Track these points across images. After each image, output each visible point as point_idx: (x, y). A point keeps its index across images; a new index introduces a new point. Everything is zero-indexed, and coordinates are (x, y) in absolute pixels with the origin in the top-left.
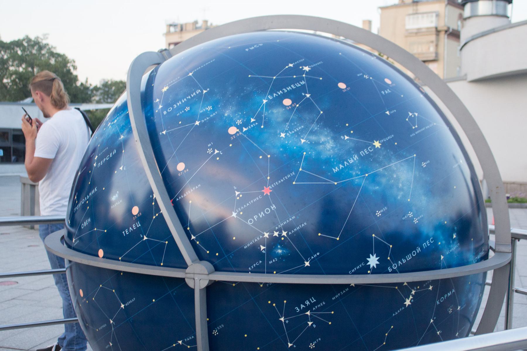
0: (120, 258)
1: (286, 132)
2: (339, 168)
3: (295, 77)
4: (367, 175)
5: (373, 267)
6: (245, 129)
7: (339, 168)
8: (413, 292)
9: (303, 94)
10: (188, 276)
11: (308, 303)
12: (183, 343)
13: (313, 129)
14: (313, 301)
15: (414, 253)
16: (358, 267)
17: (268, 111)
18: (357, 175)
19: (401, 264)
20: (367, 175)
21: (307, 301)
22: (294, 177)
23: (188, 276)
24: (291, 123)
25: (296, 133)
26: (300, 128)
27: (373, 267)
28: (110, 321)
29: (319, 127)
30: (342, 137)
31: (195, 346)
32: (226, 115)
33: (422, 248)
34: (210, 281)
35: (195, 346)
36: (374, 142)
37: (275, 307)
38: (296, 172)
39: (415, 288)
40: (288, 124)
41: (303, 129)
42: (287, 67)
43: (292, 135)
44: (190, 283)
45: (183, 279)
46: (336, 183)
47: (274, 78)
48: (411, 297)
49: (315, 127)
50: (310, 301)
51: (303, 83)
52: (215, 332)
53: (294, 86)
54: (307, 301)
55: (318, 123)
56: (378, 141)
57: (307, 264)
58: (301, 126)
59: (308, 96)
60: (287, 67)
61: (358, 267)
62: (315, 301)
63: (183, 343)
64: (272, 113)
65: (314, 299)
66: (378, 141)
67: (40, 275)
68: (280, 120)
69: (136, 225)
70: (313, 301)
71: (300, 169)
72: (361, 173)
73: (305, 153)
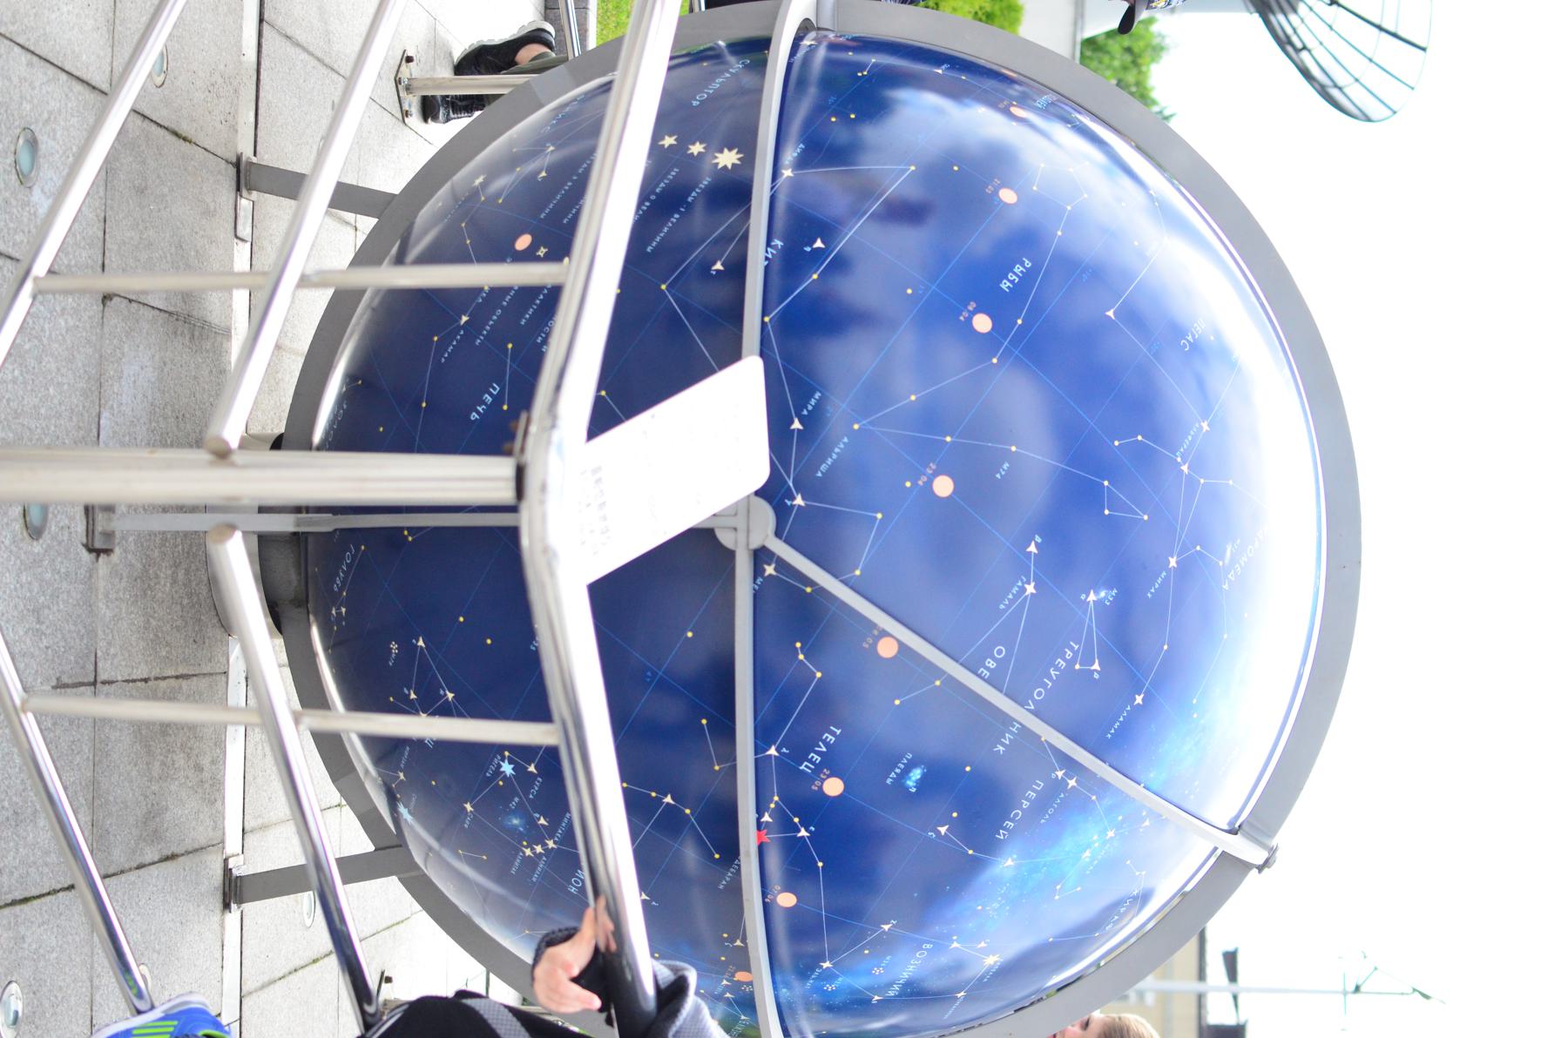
0: (603, 393)
5: (737, 153)
11: (1001, 748)
12: (796, 508)
14: (806, 766)
19: (817, 749)
21: (989, 660)
27: (737, 153)
28: (466, 322)
31: (716, 367)
35: (716, 367)
37: (816, 680)
50: (1034, 790)
52: (767, 319)
53: (814, 760)
54: (989, 660)
62: (802, 767)
63: (796, 508)
65: (806, 769)
67: (369, 51)
69: (813, 763)
70: (806, 766)
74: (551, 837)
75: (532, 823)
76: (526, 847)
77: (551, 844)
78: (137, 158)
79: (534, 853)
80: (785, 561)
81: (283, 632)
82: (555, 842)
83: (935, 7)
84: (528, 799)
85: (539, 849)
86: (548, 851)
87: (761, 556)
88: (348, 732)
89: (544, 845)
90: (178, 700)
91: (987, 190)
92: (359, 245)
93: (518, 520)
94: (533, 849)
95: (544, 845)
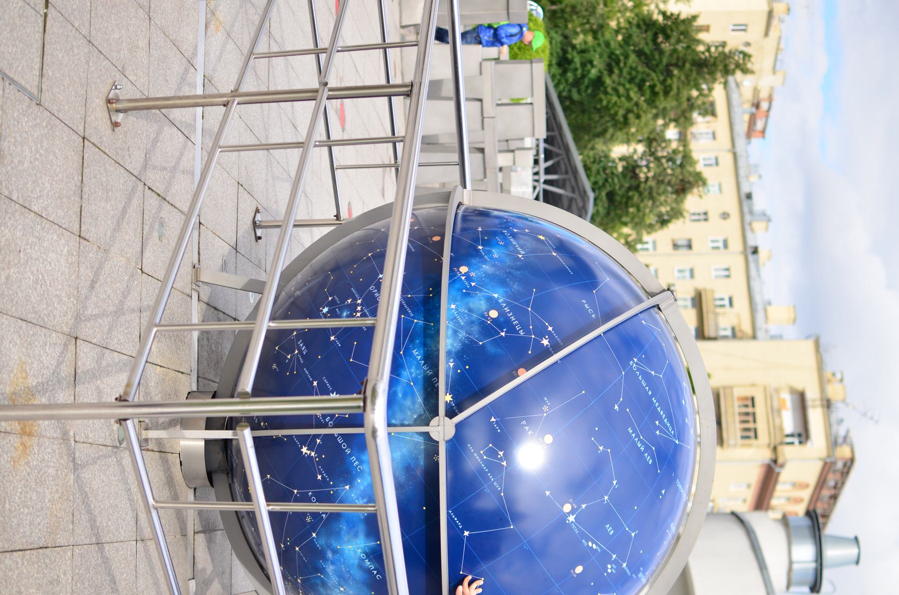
1: (456, 310)
2: (417, 355)
3: (531, 327)
4: (412, 384)
6: (463, 278)
7: (417, 355)
8: (313, 454)
9: (505, 330)
10: (442, 419)
13: (460, 333)
15: (344, 446)
16: (328, 385)
17: (482, 296)
18: (411, 374)
20: (412, 384)
22: (409, 316)
23: (442, 419)
24: (467, 314)
25: (455, 318)
26: (461, 321)
29: (462, 339)
30: (452, 360)
32: (484, 266)
33: (351, 455)
34: (438, 442)
36: (450, 394)
38: (414, 318)
39: (316, 455)
40: (466, 311)
41: (459, 323)
42: (547, 324)
43: (453, 314)
44: (434, 421)
45: (438, 415)
46: (401, 353)
47: (530, 309)
48: (308, 452)
49: (462, 334)
51: (522, 333)
55: (468, 338)
56: (452, 399)
57: (332, 338)
58: (464, 322)
59: (503, 334)
60: (547, 324)
61: (328, 385)
64: (481, 300)
66: (452, 399)
68: (472, 305)
69: (517, 325)
71: (415, 321)
72: (414, 377)
73: (432, 324)
74: (356, 300)
75: (349, 306)
76: (356, 314)
77: (359, 301)
78: (149, 157)
79: (360, 311)
80: (439, 362)
81: (215, 484)
82: (359, 299)
83: (686, 82)
84: (340, 304)
85: (359, 308)
86: (361, 304)
87: (451, 414)
88: (269, 326)
89: (358, 305)
90: (218, 331)
91: (608, 525)
92: (252, 37)
93: (252, 434)
94: (358, 311)
95: (358, 305)
